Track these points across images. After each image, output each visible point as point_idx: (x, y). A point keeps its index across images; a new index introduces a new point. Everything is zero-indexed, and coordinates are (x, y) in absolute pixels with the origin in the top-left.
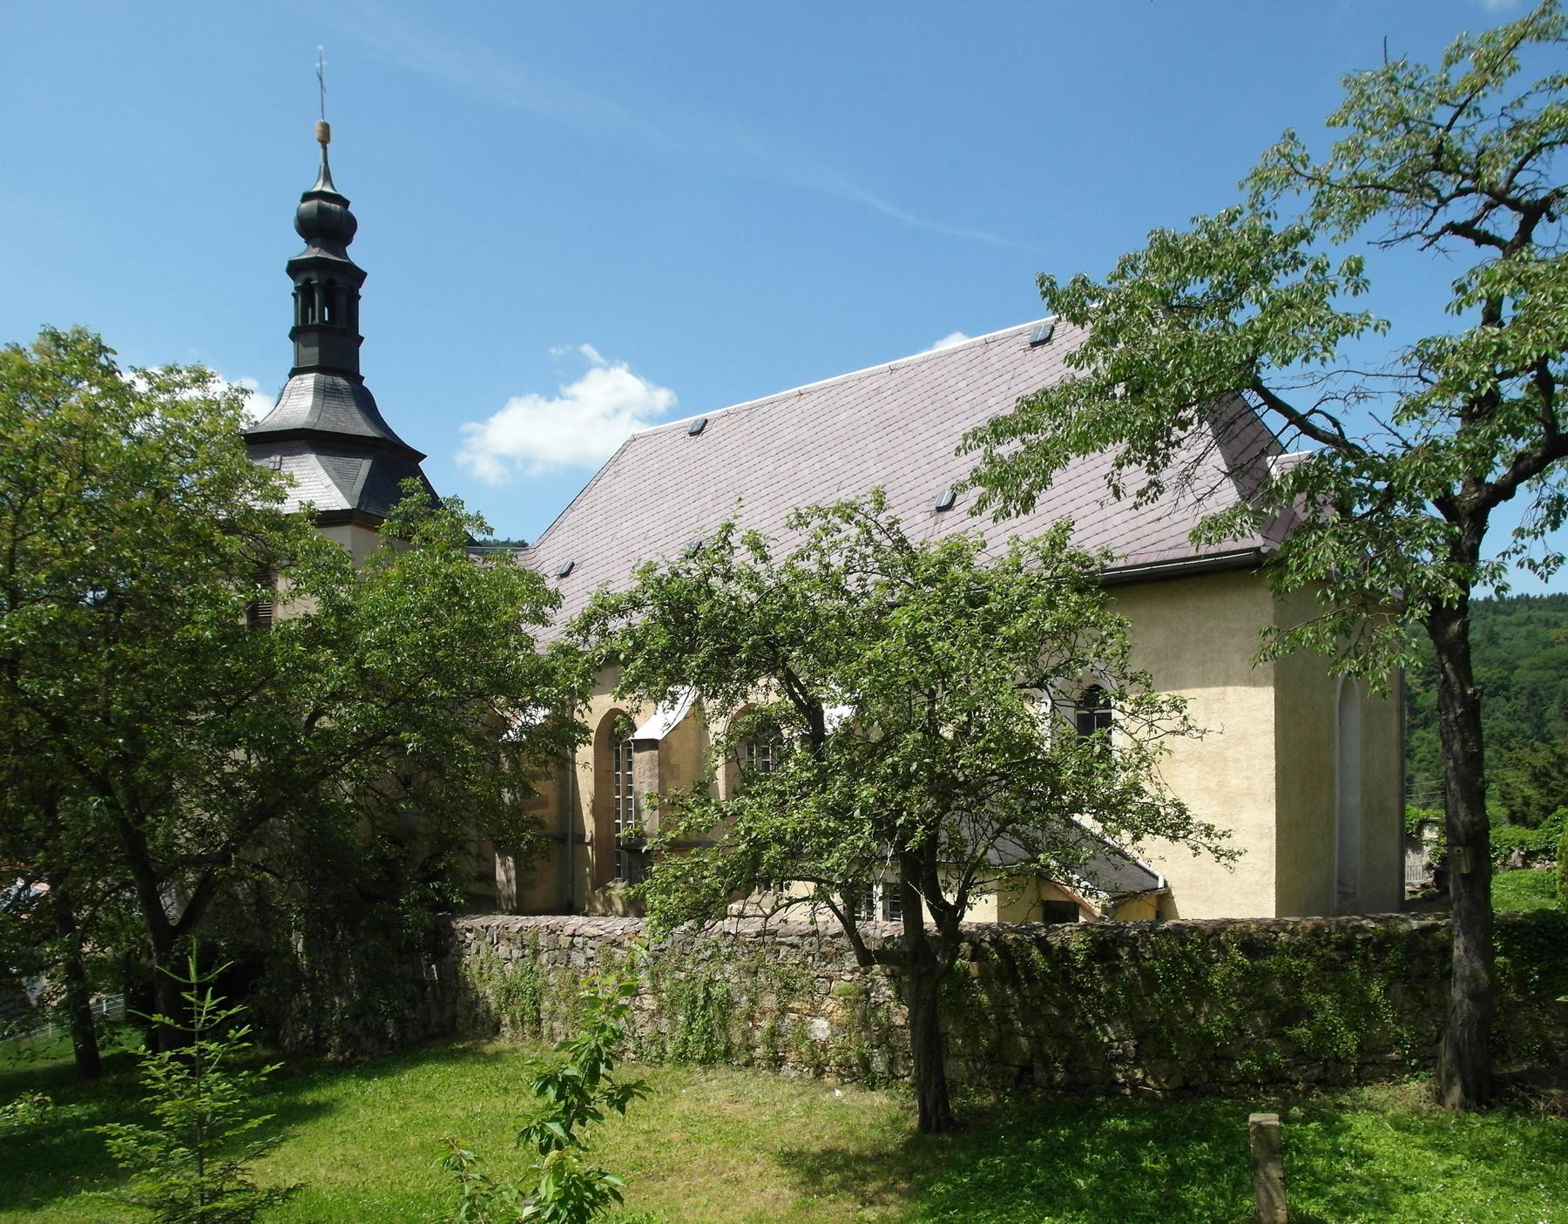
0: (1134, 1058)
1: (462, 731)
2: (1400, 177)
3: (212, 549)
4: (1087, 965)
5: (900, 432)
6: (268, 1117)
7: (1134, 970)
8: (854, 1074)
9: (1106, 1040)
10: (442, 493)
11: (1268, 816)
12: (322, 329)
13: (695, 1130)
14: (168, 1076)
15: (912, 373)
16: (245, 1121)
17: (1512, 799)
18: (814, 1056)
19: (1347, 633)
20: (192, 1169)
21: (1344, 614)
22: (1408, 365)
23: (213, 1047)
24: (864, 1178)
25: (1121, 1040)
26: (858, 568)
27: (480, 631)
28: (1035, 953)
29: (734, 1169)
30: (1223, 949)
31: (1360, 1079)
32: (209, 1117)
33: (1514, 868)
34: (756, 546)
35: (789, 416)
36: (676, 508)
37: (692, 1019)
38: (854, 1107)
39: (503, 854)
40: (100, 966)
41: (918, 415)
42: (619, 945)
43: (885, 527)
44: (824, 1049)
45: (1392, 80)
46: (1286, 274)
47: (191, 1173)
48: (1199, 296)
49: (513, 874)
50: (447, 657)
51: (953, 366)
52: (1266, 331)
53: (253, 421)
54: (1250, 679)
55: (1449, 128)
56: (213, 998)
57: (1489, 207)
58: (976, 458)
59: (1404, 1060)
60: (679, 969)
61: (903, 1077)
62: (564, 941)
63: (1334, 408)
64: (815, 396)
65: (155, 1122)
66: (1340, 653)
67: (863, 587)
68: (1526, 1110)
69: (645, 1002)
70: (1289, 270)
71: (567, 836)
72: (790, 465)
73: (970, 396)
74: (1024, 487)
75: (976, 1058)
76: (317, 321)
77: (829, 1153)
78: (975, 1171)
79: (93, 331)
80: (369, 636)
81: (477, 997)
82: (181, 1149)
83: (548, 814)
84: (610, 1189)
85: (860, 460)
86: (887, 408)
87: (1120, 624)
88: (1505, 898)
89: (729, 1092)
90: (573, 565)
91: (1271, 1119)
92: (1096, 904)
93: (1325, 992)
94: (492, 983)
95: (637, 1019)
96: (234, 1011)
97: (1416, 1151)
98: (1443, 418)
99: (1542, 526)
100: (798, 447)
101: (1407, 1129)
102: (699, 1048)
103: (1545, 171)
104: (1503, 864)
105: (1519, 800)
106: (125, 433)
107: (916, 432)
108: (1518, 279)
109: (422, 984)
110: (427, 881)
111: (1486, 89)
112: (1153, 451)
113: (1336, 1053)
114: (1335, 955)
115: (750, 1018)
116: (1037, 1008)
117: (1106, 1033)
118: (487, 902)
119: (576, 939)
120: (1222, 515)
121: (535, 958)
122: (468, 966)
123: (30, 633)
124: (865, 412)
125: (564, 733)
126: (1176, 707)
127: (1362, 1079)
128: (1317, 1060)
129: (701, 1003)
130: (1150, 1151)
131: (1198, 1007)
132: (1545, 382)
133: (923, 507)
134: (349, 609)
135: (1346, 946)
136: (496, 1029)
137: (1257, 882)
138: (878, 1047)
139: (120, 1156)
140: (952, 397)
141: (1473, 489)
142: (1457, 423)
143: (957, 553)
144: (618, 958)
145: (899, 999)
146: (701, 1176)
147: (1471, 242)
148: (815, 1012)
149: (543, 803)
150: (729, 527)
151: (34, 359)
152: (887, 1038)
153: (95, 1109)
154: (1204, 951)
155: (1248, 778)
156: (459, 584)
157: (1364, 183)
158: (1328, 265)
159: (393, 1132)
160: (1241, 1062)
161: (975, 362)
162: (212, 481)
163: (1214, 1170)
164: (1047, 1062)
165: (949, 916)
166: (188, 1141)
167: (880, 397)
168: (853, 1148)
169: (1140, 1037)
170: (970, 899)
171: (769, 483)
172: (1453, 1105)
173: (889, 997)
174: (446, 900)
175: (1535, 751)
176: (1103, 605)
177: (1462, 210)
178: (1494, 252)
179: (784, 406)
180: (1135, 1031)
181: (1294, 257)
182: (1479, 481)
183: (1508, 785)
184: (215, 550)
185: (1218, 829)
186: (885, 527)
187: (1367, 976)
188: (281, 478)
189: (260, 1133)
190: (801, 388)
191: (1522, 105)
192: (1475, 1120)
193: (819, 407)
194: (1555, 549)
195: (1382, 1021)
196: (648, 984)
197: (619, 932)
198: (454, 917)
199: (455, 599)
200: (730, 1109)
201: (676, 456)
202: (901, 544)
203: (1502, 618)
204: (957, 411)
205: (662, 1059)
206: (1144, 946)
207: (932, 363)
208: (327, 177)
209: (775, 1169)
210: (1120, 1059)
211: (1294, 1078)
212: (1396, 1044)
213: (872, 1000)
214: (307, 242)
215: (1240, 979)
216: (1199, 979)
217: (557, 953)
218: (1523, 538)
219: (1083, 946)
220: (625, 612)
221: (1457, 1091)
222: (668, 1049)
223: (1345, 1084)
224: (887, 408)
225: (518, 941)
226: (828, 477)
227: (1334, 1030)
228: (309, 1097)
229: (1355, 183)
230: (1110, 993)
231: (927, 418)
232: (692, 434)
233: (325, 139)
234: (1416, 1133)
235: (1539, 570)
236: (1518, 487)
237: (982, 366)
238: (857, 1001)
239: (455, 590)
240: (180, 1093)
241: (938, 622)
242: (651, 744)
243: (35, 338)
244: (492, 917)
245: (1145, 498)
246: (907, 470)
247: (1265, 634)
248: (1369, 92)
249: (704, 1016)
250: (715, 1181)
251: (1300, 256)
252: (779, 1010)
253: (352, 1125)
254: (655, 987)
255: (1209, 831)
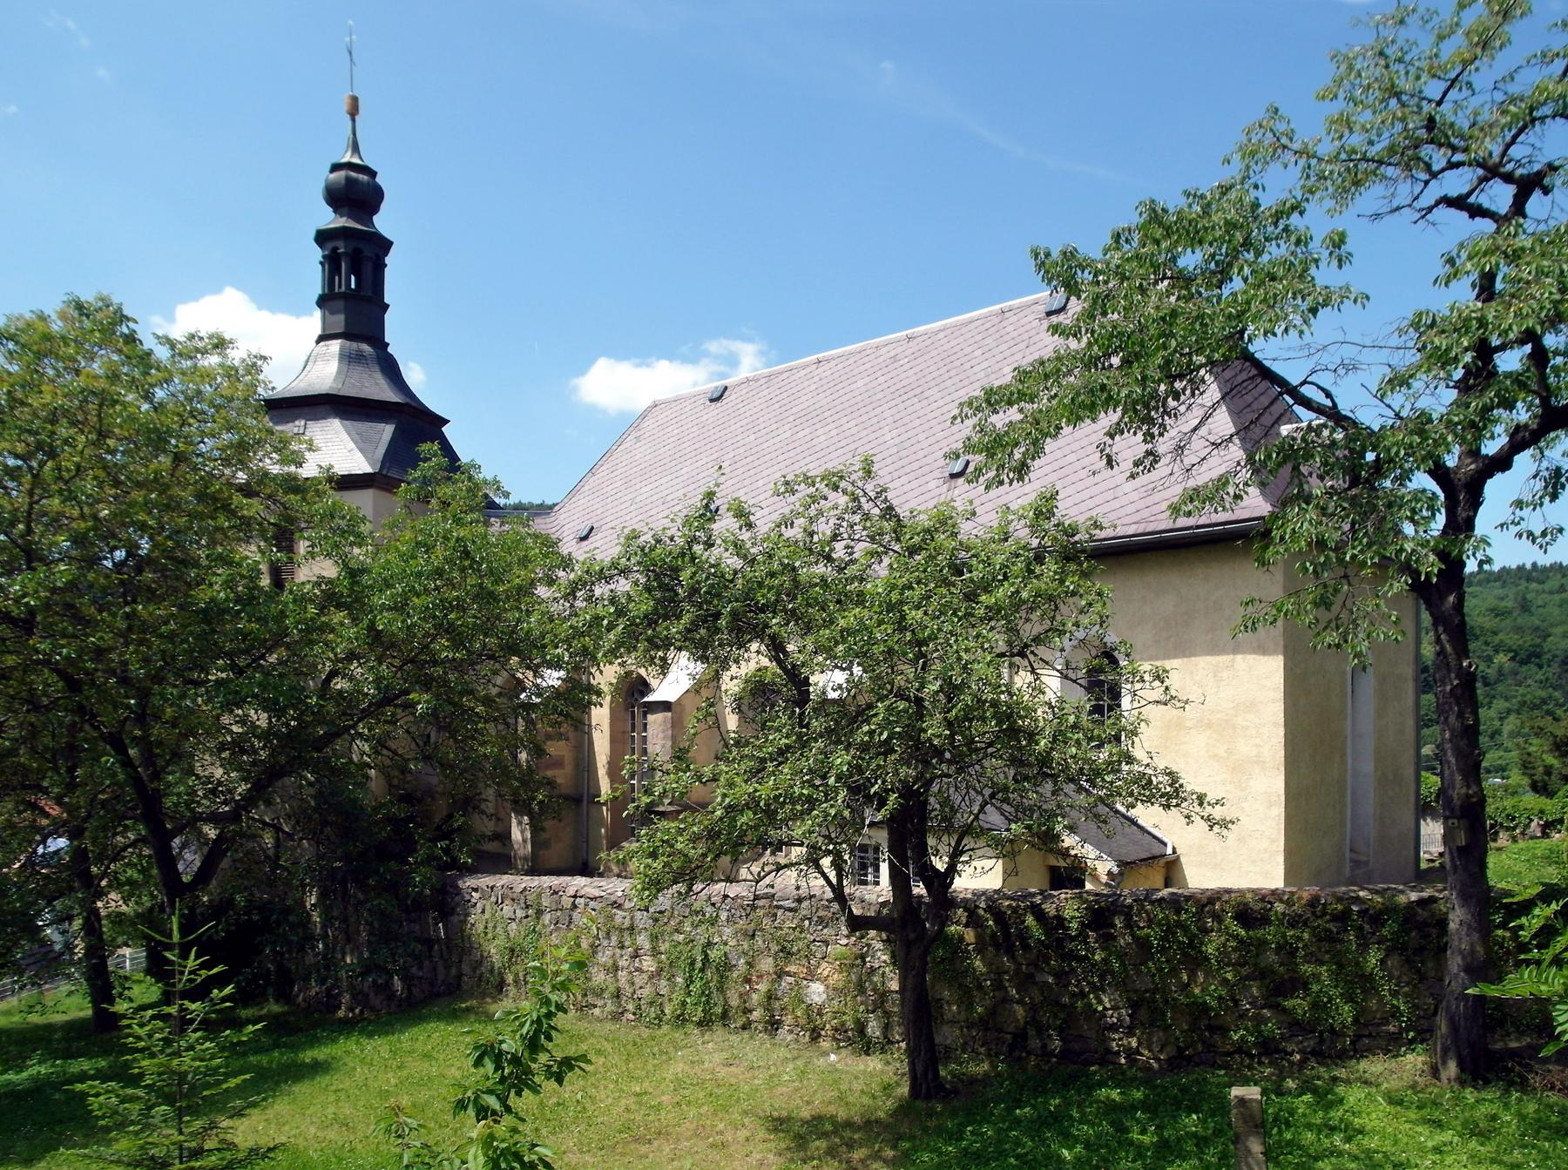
0: (1128, 1027)
1: (471, 692)
2: (1392, 150)
3: (226, 508)
4: (1082, 936)
5: (916, 400)
6: (248, 1076)
7: (1129, 939)
8: (850, 1039)
9: (1100, 1008)
10: (464, 457)
11: (1275, 784)
12: (348, 296)
13: (687, 1093)
14: (150, 1036)
15: (929, 341)
16: (225, 1081)
17: (1534, 768)
18: (810, 1019)
19: (1328, 606)
20: (173, 1127)
21: (1325, 586)
22: (1404, 337)
23: (193, 1006)
24: (850, 1145)
25: (1114, 1008)
26: (845, 536)
27: (491, 594)
28: (1030, 920)
29: (721, 1133)
30: (1218, 918)
31: (1356, 1051)
32: (190, 1076)
33: (1532, 838)
34: (741, 514)
35: (806, 383)
36: (694, 473)
37: (690, 981)
38: (847, 1072)
39: (519, 813)
40: (118, 919)
41: (933, 383)
42: (620, 907)
43: (872, 495)
44: (820, 1014)
45: (1381, 54)
46: (1278, 246)
47: (171, 1132)
48: (1191, 269)
49: (528, 835)
50: (459, 619)
51: (969, 335)
52: (1248, 303)
53: (270, 386)
54: (1259, 647)
55: (1439, 103)
56: (197, 958)
57: (1483, 180)
58: (967, 428)
59: (1401, 1034)
60: (677, 931)
61: (898, 1042)
62: (567, 902)
63: (1325, 379)
64: (833, 363)
65: (135, 1080)
66: (1321, 627)
67: (851, 554)
68: (1524, 1086)
69: (645, 963)
70: (1281, 242)
71: (582, 796)
72: (807, 431)
73: (985, 364)
74: (1017, 456)
75: (971, 1025)
76: (343, 288)
77: (818, 1119)
78: (961, 1139)
79: (116, 300)
80: (380, 600)
81: (482, 956)
82: (164, 1107)
83: (562, 776)
84: (541, 1159)
85: (876, 427)
86: (903, 376)
87: (1100, 594)
88: (1517, 869)
89: (725, 1055)
90: (592, 528)
91: (1253, 1092)
92: (1104, 866)
93: (1322, 963)
94: (496, 942)
95: (637, 980)
96: (215, 971)
97: (1408, 1126)
98: (1427, 391)
99: (1541, 498)
100: (814, 414)
101: (1400, 1103)
102: (696, 1010)
103: (1538, 145)
104: (1523, 833)
105: (1541, 769)
106: (148, 397)
107: (932, 399)
108: (1505, 253)
109: (429, 942)
110: (434, 840)
111: (1477, 63)
112: (1150, 421)
113: (1331, 1025)
114: (1331, 926)
115: (748, 981)
116: (1032, 976)
117: (1100, 1002)
118: (501, 861)
119: (578, 900)
120: (1205, 486)
121: (538, 918)
122: (473, 925)
123: (42, 594)
124: (881, 380)
125: (576, 697)
126: (1158, 677)
127: (1358, 1052)
128: (1313, 1032)
129: (699, 965)
130: (1138, 1121)
131: (1193, 976)
132: (1540, 357)
133: (937, 474)
134: (364, 570)
135: (1343, 917)
136: (501, 986)
137: (1265, 850)
138: (873, 1012)
139: (100, 1113)
140: (967, 366)
141: (1469, 460)
142: (1453, 394)
143: (945, 522)
144: (618, 920)
145: (894, 964)
146: (688, 1139)
147: (1465, 215)
148: (812, 976)
149: (559, 763)
150: (710, 495)
151: (57, 326)
152: (882, 1003)
153: (103, 1063)
154: (1199, 920)
155: (1258, 746)
156: (470, 547)
157: (1354, 157)
158: (1311, 238)
159: (387, 1091)
160: (1235, 1032)
161: (990, 331)
162: (231, 446)
163: (1202, 1142)
164: (1041, 1030)
165: (940, 882)
166: (169, 1099)
167: (896, 365)
168: (842, 1114)
169: (1134, 1006)
170: (959, 867)
171: (786, 449)
172: (1449, 1080)
173: (885, 962)
174: (455, 860)
175: (1557, 719)
176: (1085, 575)
177: (1457, 183)
178: (1488, 225)
179: (803, 373)
180: (1129, 999)
181: (1286, 229)
182: (1474, 453)
183: (1529, 754)
184: (233, 513)
185: (1211, 797)
186: (872, 495)
187: (1364, 947)
188: (300, 442)
189: (240, 1091)
190: (820, 356)
191: (1513, 79)
192: (1470, 1095)
193: (837, 374)
194: (1554, 522)
195: (1378, 993)
196: (647, 946)
197: (620, 894)
198: (462, 876)
199: (467, 563)
200: (723, 1072)
201: (696, 422)
202: (889, 512)
203: (1534, 585)
204: (972, 379)
205: (661, 1021)
206: (1139, 915)
207: (949, 331)
208: (355, 148)
209: (762, 1134)
210: (1113, 1028)
211: (1289, 1049)
212: (1393, 1016)
213: (868, 965)
214: (335, 212)
215: (1235, 949)
216: (1194, 948)
217: (559, 913)
218: (1521, 509)
219: (1077, 914)
220: (611, 577)
221: (1452, 1068)
222: (667, 1011)
223: (1342, 1057)
224: (903, 376)
225: (522, 901)
226: (843, 443)
227: (1329, 1002)
228: (308, 1056)
229: (1343, 156)
230: (1105, 961)
231: (942, 386)
232: (712, 400)
233: (354, 111)
234: (1408, 1108)
235: (1538, 540)
236: (1516, 458)
237: (998, 335)
238: (852, 966)
239: (467, 554)
240: (162, 1052)
241: (919, 591)
242: (665, 706)
243: (59, 306)
244: (498, 876)
245: (1141, 468)
246: (922, 437)
247: (1247, 604)
248: (1358, 66)
249: (702, 978)
250: (701, 1146)
251: (1292, 228)
252: (776, 973)
253: (347, 1083)
254: (654, 948)
255: (1201, 799)
